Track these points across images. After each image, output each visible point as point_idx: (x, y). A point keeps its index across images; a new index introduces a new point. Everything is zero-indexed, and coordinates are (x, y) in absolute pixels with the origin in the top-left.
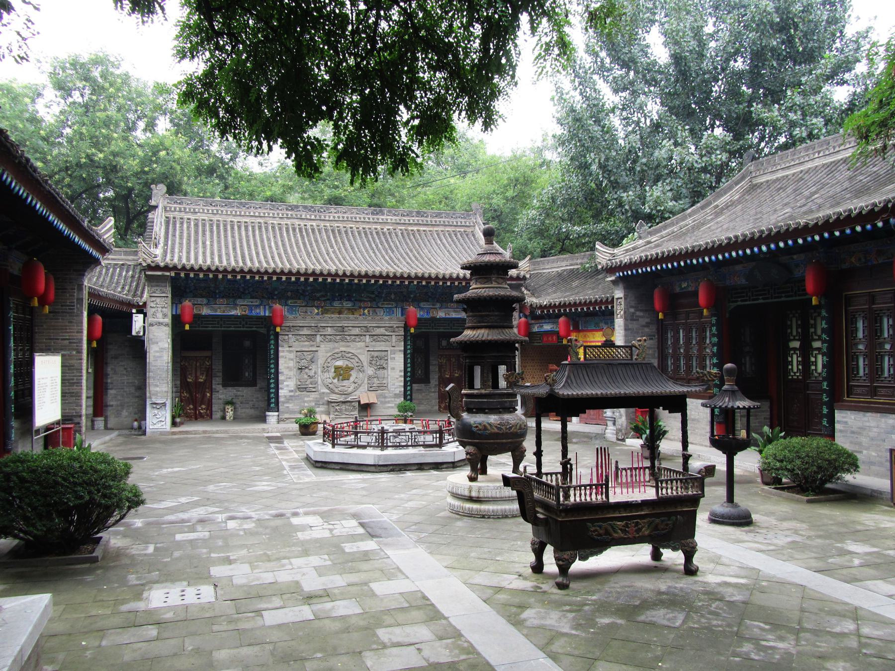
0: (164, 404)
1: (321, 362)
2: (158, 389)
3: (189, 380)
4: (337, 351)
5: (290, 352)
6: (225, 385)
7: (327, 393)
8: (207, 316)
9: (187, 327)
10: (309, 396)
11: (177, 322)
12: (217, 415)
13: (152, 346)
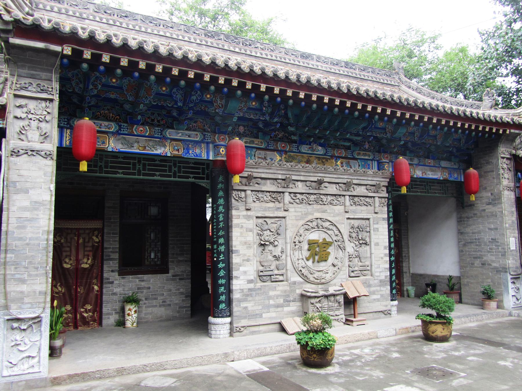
0: (38, 320)
1: (290, 234)
2: (24, 288)
3: (65, 266)
4: (310, 217)
5: (248, 217)
6: (122, 273)
7: (302, 283)
8: (115, 155)
9: (84, 167)
10: (275, 289)
11: (66, 159)
12: (110, 319)
13: (15, 197)
